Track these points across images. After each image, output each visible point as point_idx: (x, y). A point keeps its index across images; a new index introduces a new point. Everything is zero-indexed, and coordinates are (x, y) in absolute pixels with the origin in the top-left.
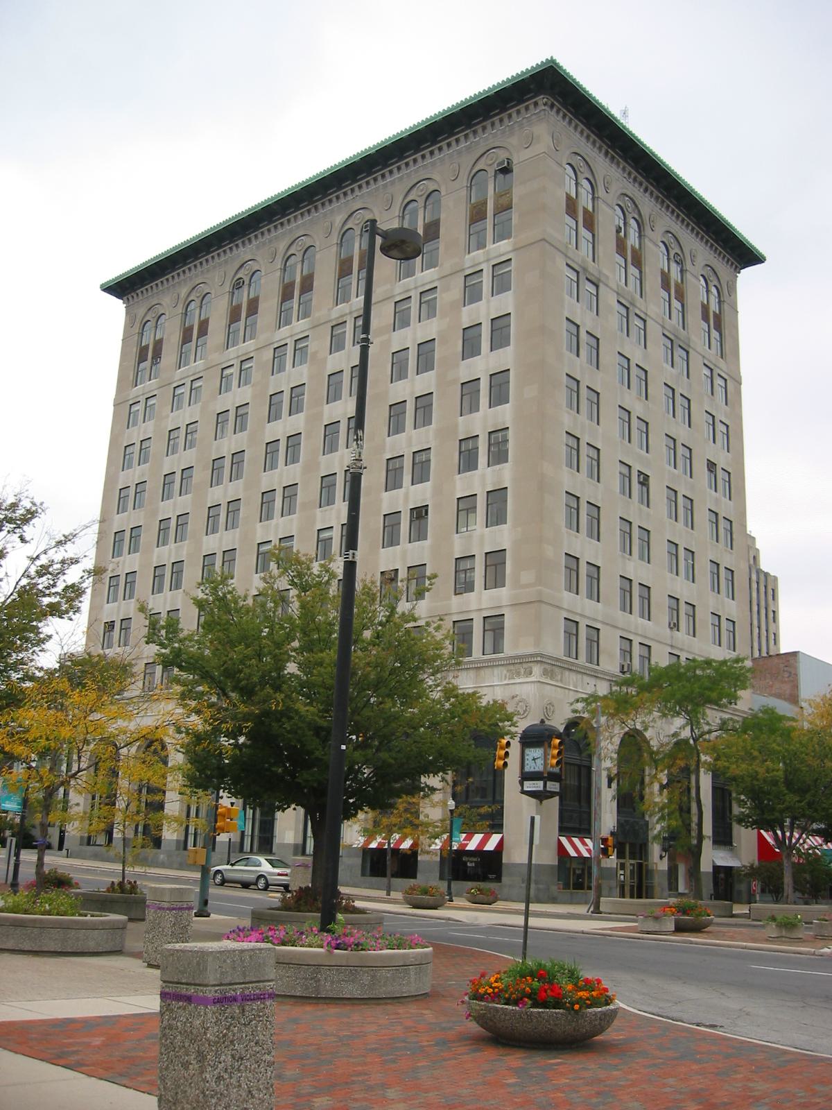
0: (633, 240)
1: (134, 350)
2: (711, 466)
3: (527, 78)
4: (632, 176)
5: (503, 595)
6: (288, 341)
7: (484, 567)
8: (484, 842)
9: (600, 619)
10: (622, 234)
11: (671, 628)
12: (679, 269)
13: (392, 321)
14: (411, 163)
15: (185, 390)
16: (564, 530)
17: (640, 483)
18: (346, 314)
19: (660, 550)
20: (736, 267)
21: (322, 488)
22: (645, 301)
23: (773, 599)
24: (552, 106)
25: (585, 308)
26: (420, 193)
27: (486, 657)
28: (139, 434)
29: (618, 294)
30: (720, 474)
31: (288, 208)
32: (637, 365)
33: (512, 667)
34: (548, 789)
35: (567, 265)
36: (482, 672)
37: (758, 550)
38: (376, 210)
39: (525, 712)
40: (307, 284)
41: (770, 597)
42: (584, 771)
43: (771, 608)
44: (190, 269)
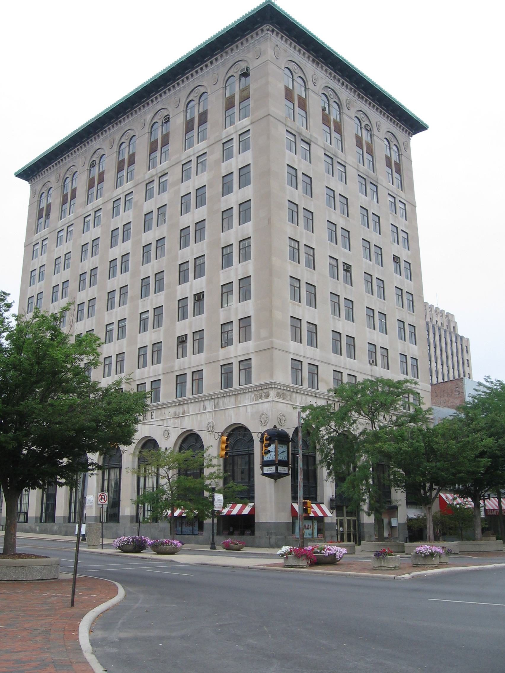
0: (334, 116)
1: (36, 212)
2: (396, 259)
3: (255, 14)
4: (333, 75)
5: (250, 345)
6: (121, 196)
7: (238, 329)
8: (242, 509)
9: (318, 359)
10: (327, 112)
11: (371, 364)
12: (369, 135)
13: (181, 177)
14: (190, 77)
15: (64, 233)
16: (289, 300)
17: (344, 270)
18: (153, 176)
19: (360, 313)
20: (409, 133)
21: (142, 286)
22: (345, 154)
23: (467, 352)
24: (273, 31)
25: (300, 158)
26: (196, 95)
27: (241, 387)
28: (38, 263)
29: (324, 149)
30: (403, 264)
31: (120, 113)
32: (340, 194)
33: (256, 393)
34: (279, 471)
35: (287, 131)
36: (239, 397)
37: (456, 323)
38: (170, 109)
39: (265, 421)
40: (132, 161)
41: (465, 351)
42: (311, 460)
43: (466, 358)
44: (65, 158)
